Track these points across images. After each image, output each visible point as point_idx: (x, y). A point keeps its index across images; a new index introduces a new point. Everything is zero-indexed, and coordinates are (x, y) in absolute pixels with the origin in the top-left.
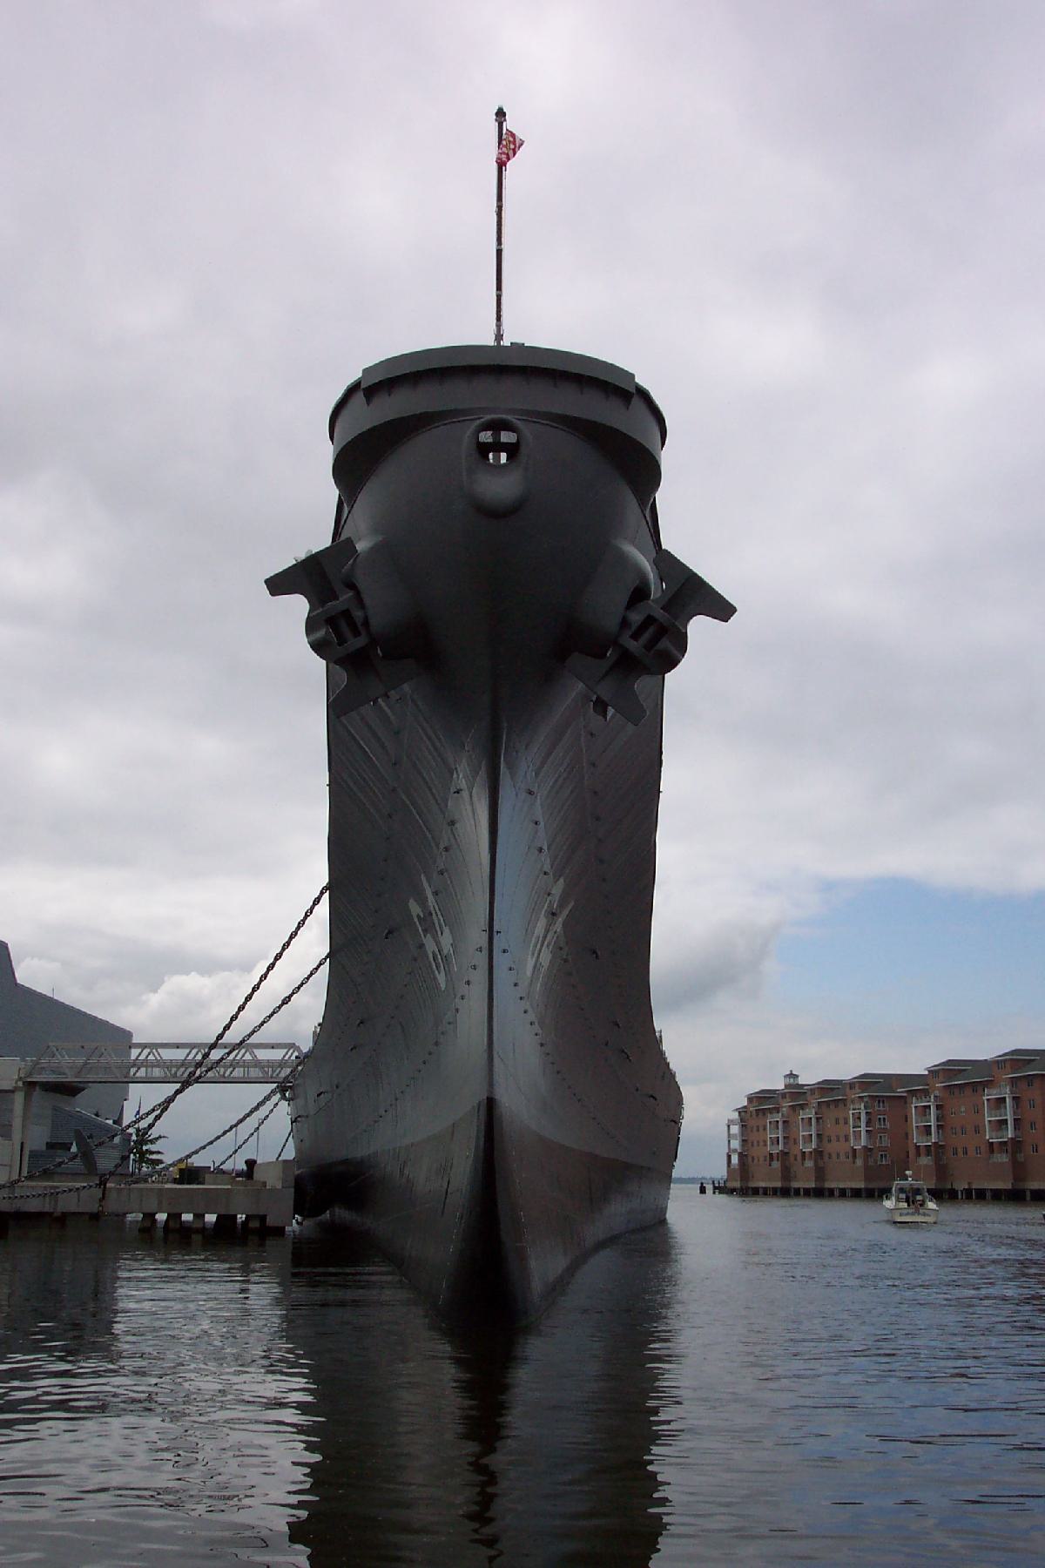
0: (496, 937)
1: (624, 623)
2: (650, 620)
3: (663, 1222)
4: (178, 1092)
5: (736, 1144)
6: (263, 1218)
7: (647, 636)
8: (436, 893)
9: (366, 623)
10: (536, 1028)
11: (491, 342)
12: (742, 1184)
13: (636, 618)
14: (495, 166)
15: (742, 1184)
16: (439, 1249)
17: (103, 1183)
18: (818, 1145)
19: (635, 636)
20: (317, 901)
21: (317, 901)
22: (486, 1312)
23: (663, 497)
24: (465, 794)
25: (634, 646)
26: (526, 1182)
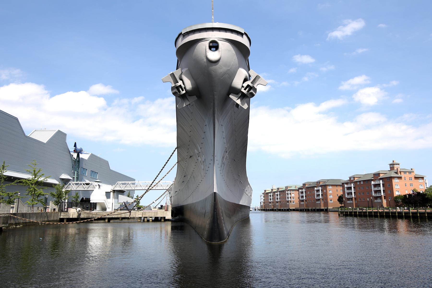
0: (215, 157)
1: (243, 87)
2: (248, 86)
3: (249, 218)
4: (146, 192)
5: (263, 200)
6: (165, 217)
7: (248, 89)
8: (201, 148)
9: (185, 88)
10: (223, 177)
11: (168, 227)
12: (264, 209)
13: (245, 85)
14: (166, 222)
15: (264, 209)
16: (205, 222)
17: (130, 212)
18: (276, 203)
19: (245, 89)
20: (175, 151)
21: (175, 151)
22: (215, 234)
23: (250, 58)
24: (207, 126)
25: (245, 92)
26: (221, 208)
